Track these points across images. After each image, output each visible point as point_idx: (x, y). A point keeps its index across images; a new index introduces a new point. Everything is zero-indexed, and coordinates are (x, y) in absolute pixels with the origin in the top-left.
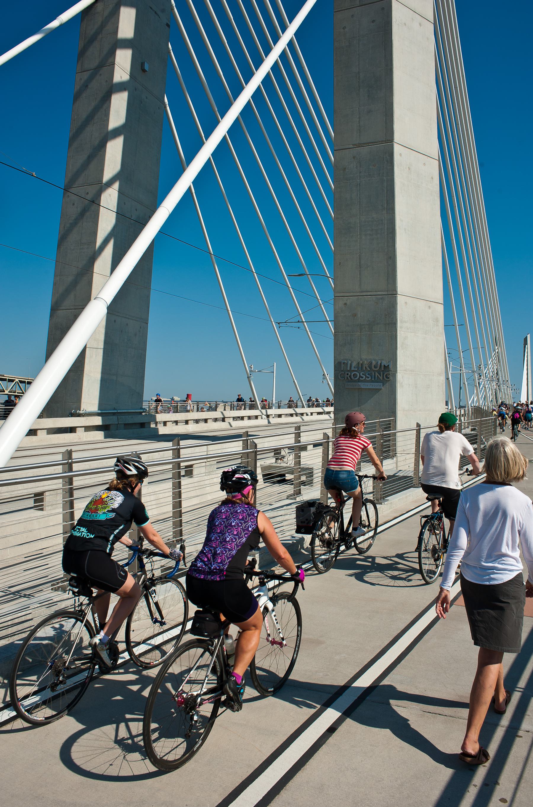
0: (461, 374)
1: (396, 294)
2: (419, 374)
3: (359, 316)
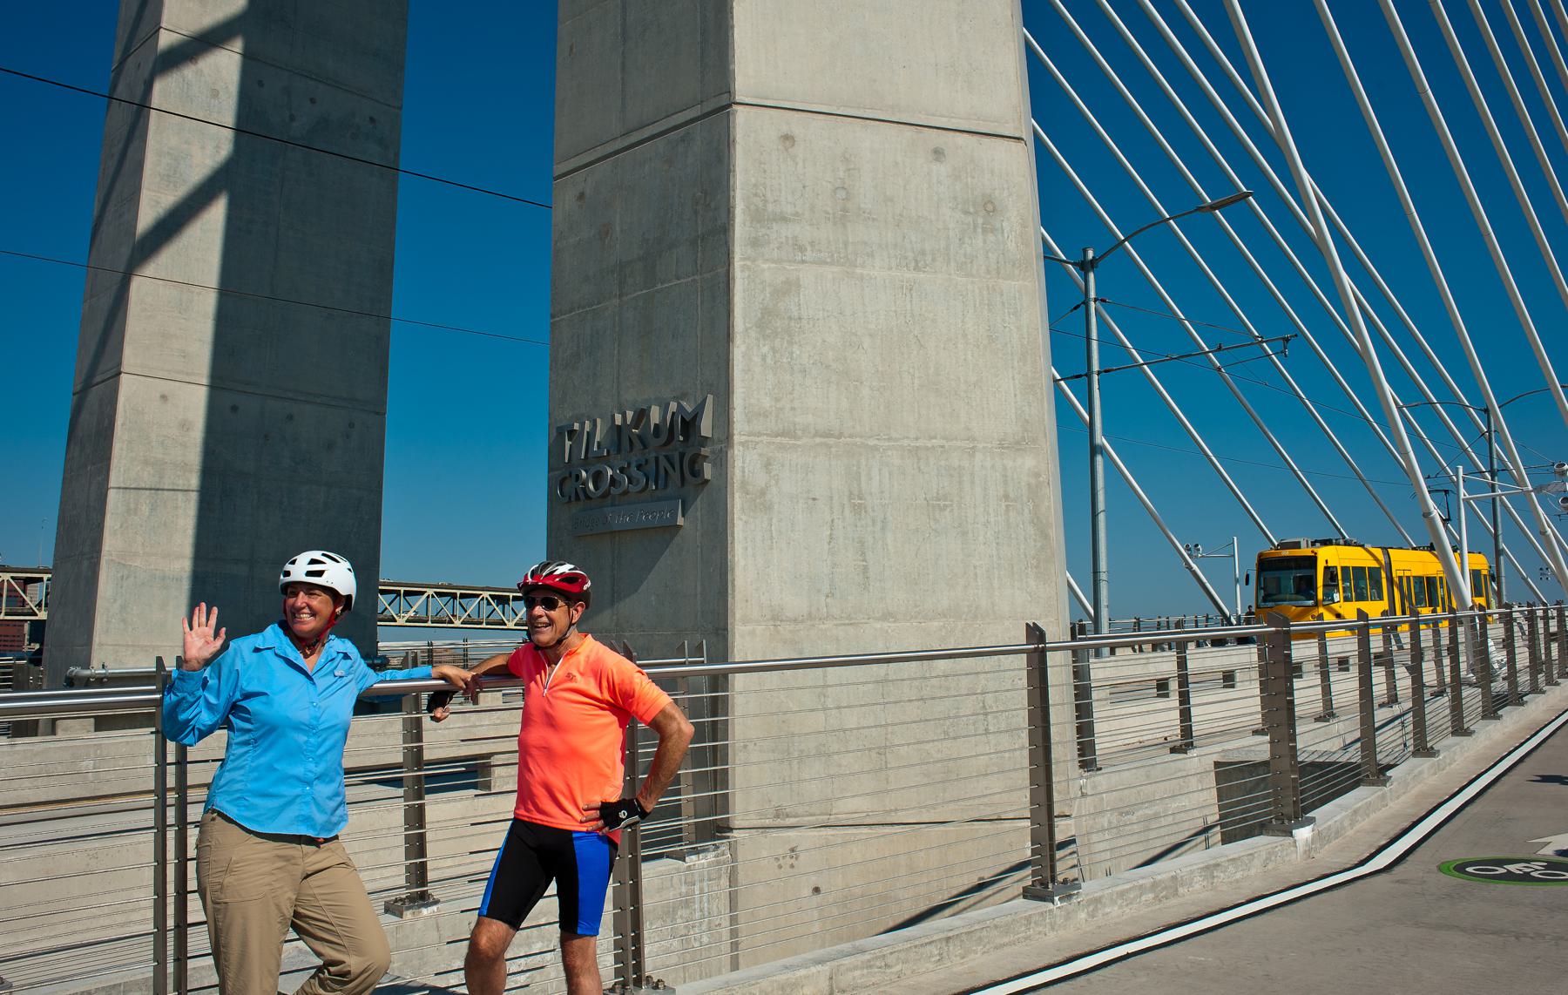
0: (1494, 500)
1: (729, 106)
2: (875, 448)
3: (618, 229)
